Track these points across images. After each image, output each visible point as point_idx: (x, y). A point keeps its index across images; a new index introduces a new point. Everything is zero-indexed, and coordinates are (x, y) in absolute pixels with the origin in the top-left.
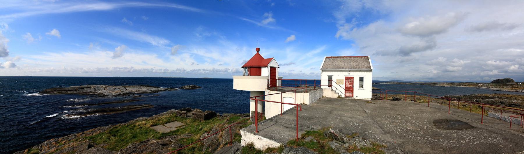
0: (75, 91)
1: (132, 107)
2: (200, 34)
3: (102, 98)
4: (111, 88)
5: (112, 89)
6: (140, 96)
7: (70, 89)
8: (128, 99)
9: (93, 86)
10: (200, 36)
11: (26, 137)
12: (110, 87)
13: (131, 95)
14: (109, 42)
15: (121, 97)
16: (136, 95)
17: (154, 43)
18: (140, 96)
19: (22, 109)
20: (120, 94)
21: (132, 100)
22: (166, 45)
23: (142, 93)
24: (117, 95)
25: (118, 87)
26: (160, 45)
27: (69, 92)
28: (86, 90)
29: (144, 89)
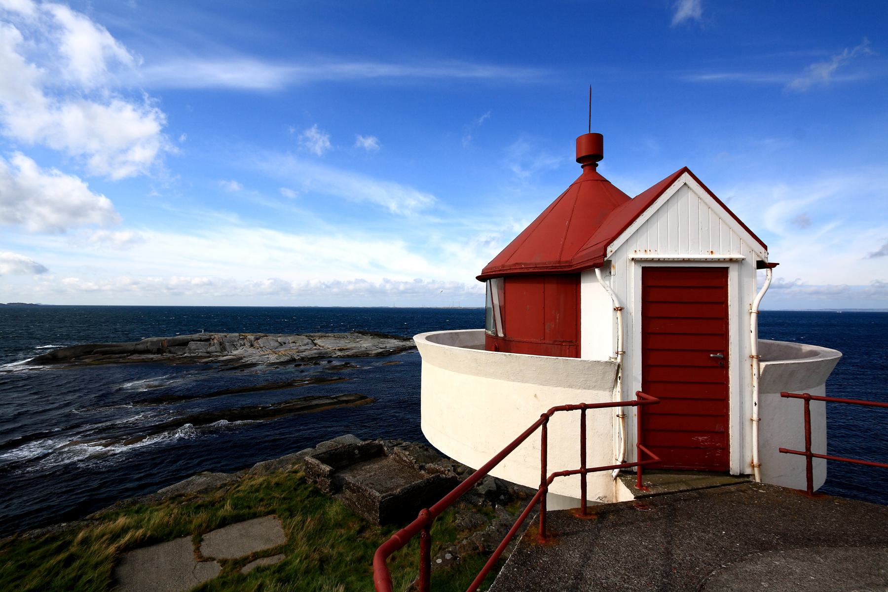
0: (160, 351)
1: (305, 404)
2: (525, 166)
3: (238, 373)
4: (271, 340)
5: (274, 344)
6: (346, 365)
7: (140, 347)
8: (312, 371)
9: (217, 336)
10: (527, 174)
11: (25, 498)
12: (271, 337)
13: (324, 363)
14: (263, 203)
15: (291, 368)
16: (335, 363)
17: (393, 206)
18: (346, 365)
19: (50, 410)
20: (292, 360)
21: (319, 380)
22: (423, 212)
23: (355, 356)
24: (282, 363)
25: (290, 339)
26: (407, 212)
27: (135, 357)
28: (196, 349)
29: (366, 344)
